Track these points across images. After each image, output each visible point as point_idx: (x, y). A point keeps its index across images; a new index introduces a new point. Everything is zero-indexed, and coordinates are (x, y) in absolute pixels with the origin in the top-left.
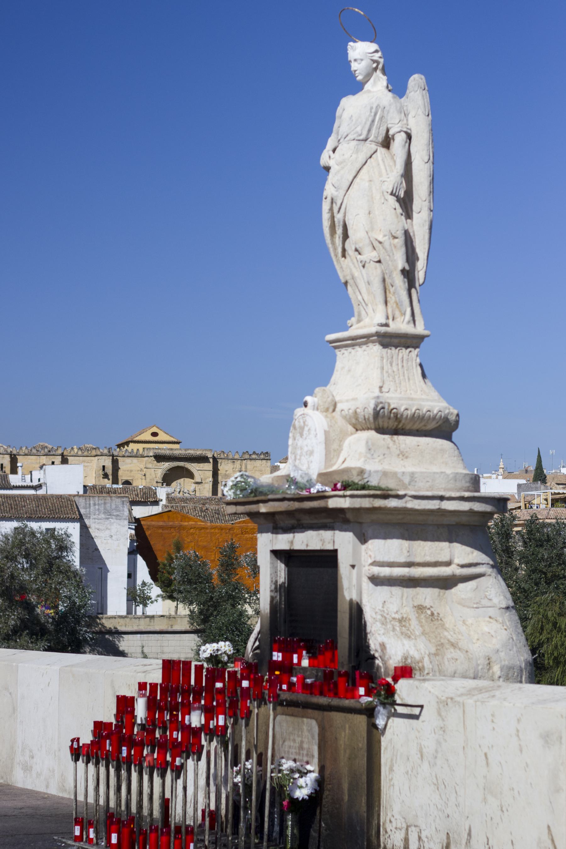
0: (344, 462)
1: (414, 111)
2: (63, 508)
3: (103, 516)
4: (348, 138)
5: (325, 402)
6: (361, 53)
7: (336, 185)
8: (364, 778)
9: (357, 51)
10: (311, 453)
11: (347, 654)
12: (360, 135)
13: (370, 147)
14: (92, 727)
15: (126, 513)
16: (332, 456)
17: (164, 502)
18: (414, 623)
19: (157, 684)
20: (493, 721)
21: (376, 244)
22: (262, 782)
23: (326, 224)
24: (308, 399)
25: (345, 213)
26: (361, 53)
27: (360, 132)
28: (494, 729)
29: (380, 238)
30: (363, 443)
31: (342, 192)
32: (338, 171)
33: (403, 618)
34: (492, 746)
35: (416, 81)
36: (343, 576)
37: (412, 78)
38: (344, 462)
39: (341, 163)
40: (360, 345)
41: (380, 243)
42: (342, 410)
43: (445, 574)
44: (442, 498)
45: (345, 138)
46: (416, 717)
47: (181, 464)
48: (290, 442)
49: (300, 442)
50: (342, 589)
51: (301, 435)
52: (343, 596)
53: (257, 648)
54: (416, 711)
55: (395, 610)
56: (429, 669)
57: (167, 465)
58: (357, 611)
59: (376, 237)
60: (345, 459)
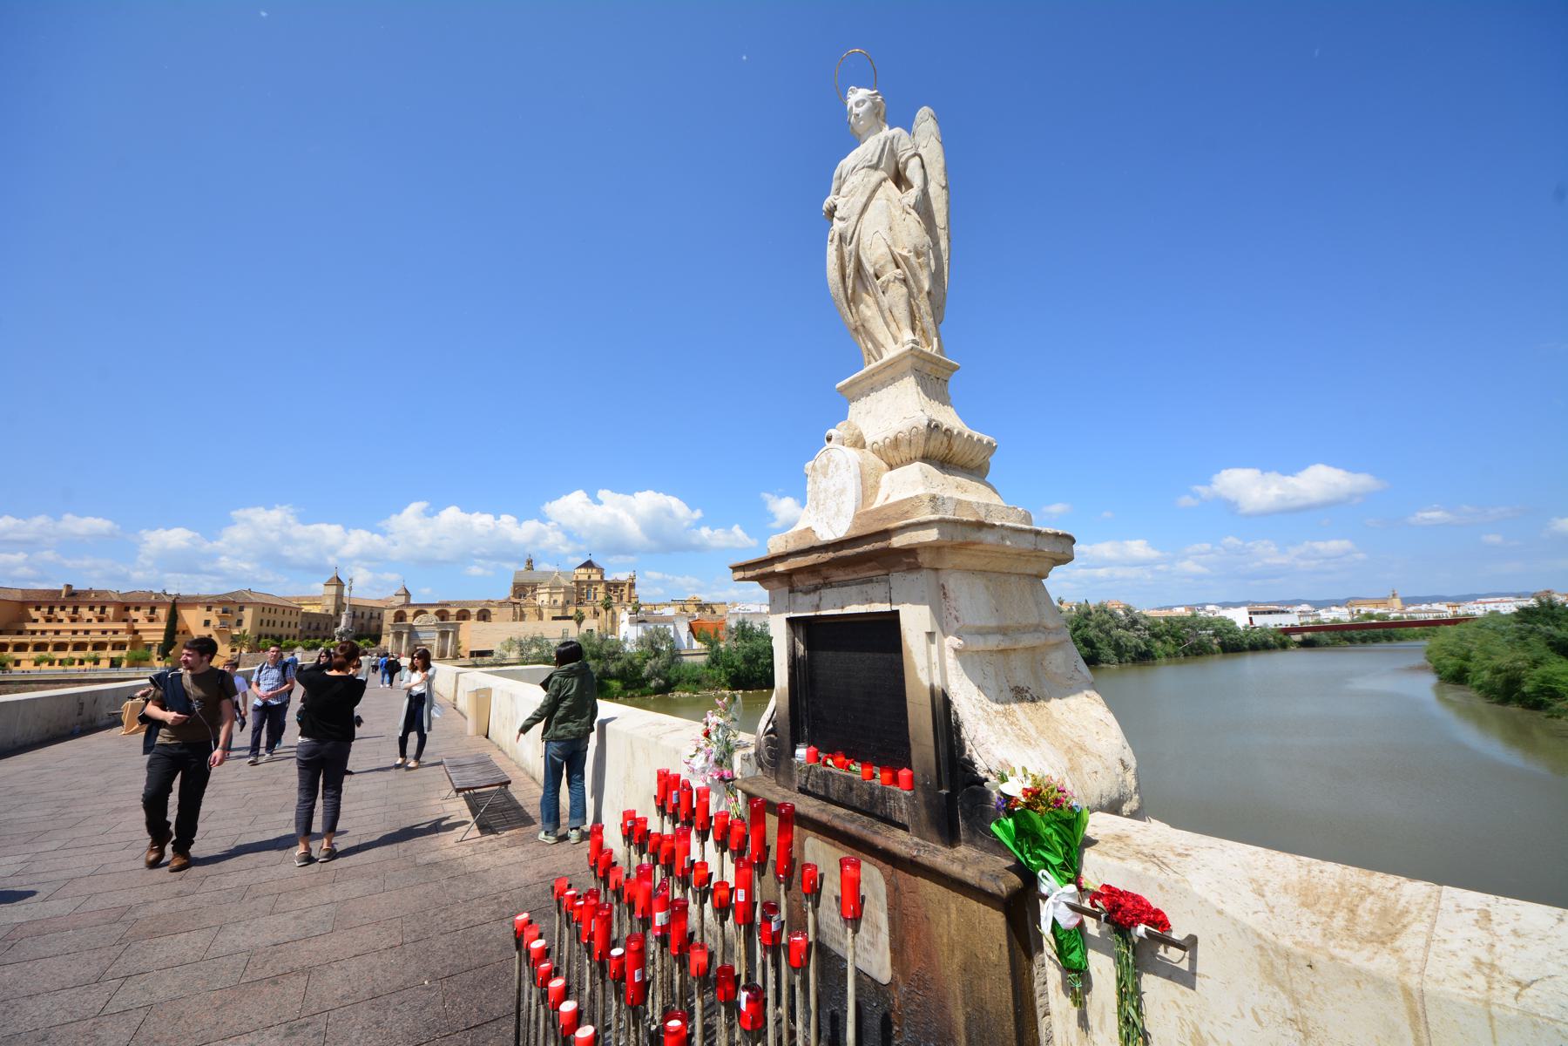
1: (924, 142)
2: (669, 620)
6: (858, 98)
8: (1010, 1026)
10: (842, 492)
11: (934, 773)
13: (881, 174)
14: (654, 788)
22: (827, 1032)
23: (832, 273)
24: (832, 431)
25: (858, 245)
26: (858, 98)
29: (905, 253)
35: (924, 112)
36: (914, 649)
40: (884, 385)
43: (36, 591)
48: (809, 488)
49: (823, 483)
50: (914, 668)
51: (825, 475)
52: (918, 681)
53: (771, 732)
58: (942, 706)
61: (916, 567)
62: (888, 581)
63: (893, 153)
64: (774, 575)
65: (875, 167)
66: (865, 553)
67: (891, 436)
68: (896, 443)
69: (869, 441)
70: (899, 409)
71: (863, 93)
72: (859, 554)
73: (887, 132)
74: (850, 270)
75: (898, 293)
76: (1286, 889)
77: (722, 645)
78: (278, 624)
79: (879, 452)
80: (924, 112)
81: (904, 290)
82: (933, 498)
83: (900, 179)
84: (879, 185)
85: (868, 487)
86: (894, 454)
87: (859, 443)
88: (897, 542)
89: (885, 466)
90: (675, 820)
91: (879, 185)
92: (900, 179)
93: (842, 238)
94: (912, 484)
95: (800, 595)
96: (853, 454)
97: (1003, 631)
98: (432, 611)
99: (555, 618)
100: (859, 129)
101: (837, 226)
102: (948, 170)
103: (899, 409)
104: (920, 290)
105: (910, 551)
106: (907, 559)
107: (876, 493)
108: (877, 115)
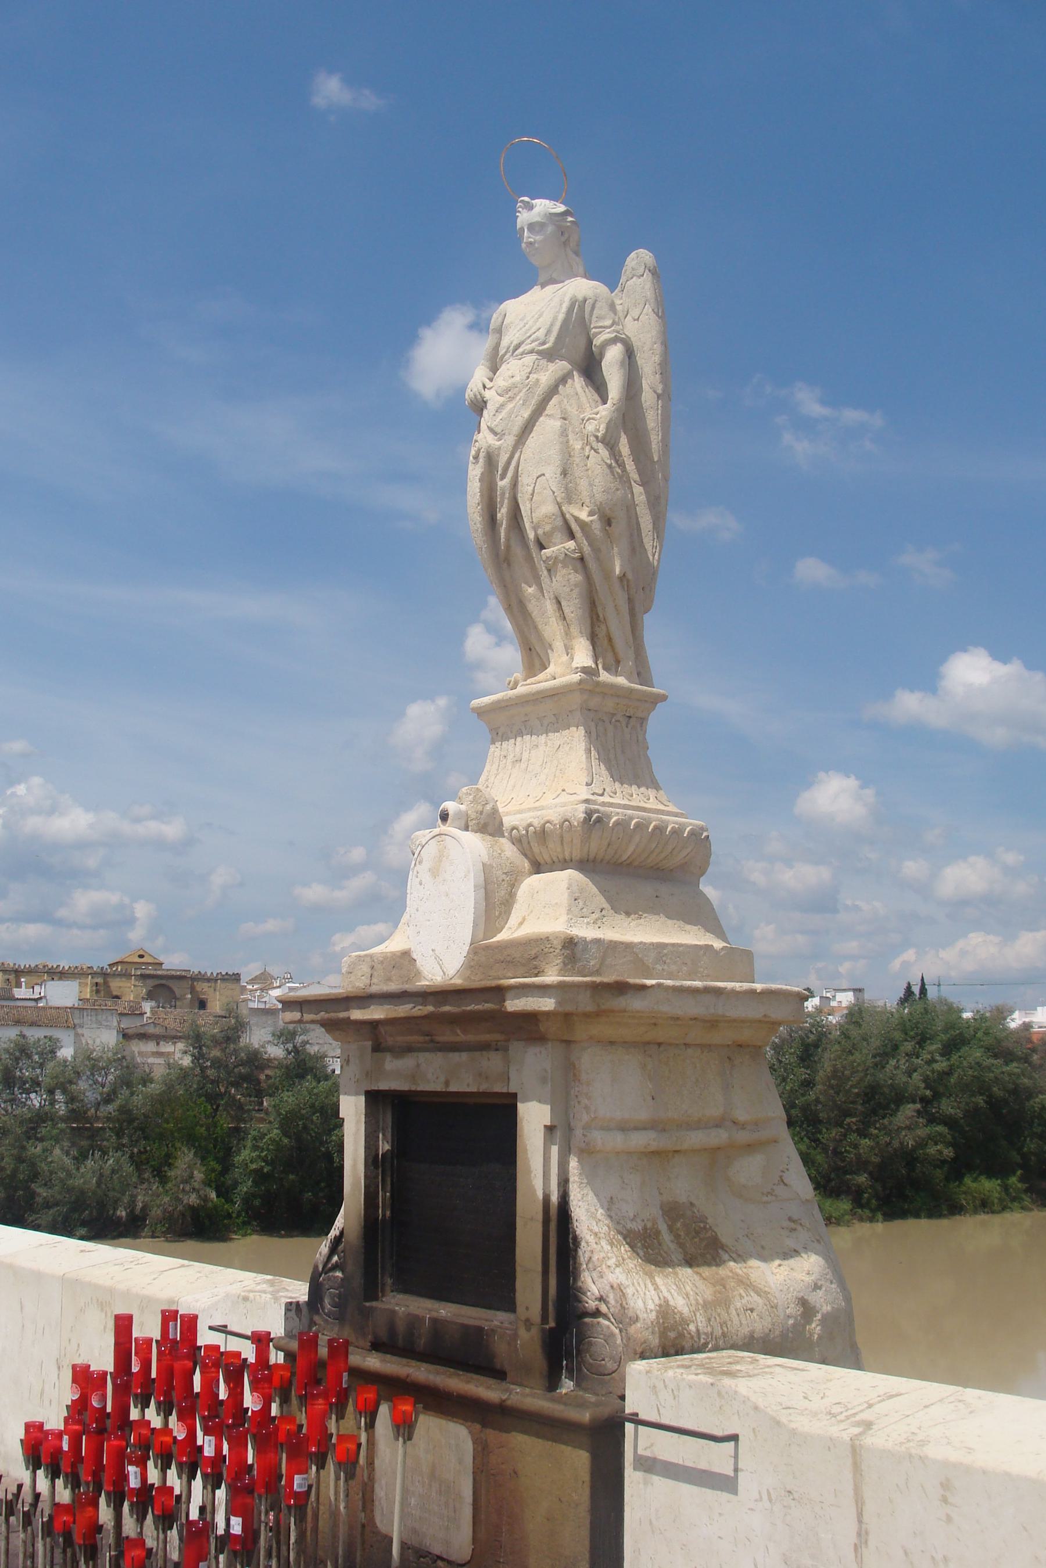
0: (521, 923)
1: (631, 311)
3: (94, 1026)
4: (520, 350)
5: (481, 813)
7: (498, 430)
9: (536, 210)
12: (544, 343)
15: (115, 1024)
16: (497, 913)
17: (148, 1015)
18: (666, 1237)
19: (105, 1373)
20: (945, 1500)
27: (542, 338)
28: (949, 1519)
29: (583, 515)
30: (565, 885)
31: (510, 440)
32: (502, 406)
33: (645, 1228)
34: (946, 1559)
37: (633, 255)
38: (521, 923)
39: (508, 390)
42: (512, 829)
45: (514, 351)
46: (727, 1484)
47: (163, 982)
52: (532, 1190)
54: (715, 1458)
55: (631, 1215)
56: (705, 1334)
57: (151, 983)
58: (560, 1223)
59: (576, 513)
60: (524, 919)
61: (540, 1039)
62: (506, 1049)
63: (583, 324)
64: (348, 1021)
65: (550, 355)
66: (471, 1012)
67: (536, 823)
68: (542, 834)
69: (508, 821)
70: (550, 780)
71: (543, 207)
72: (464, 1013)
73: (581, 287)
74: (503, 513)
75: (566, 582)
76: (690, 1387)
77: (243, 1055)
79: (517, 841)
80: (639, 259)
81: (579, 578)
82: (570, 944)
83: (590, 368)
84: (553, 391)
85: (495, 899)
86: (540, 850)
87: (488, 824)
88: (514, 1005)
89: (527, 864)
90: (74, 1483)
91: (553, 391)
92: (590, 368)
93: (491, 460)
94: (550, 907)
95: (388, 1057)
96: (473, 846)
97: (654, 1125)
100: (536, 261)
101: (484, 439)
102: (665, 368)
103: (550, 780)
104: (607, 574)
105: (531, 1018)
106: (528, 1027)
107: (508, 913)
108: (565, 244)
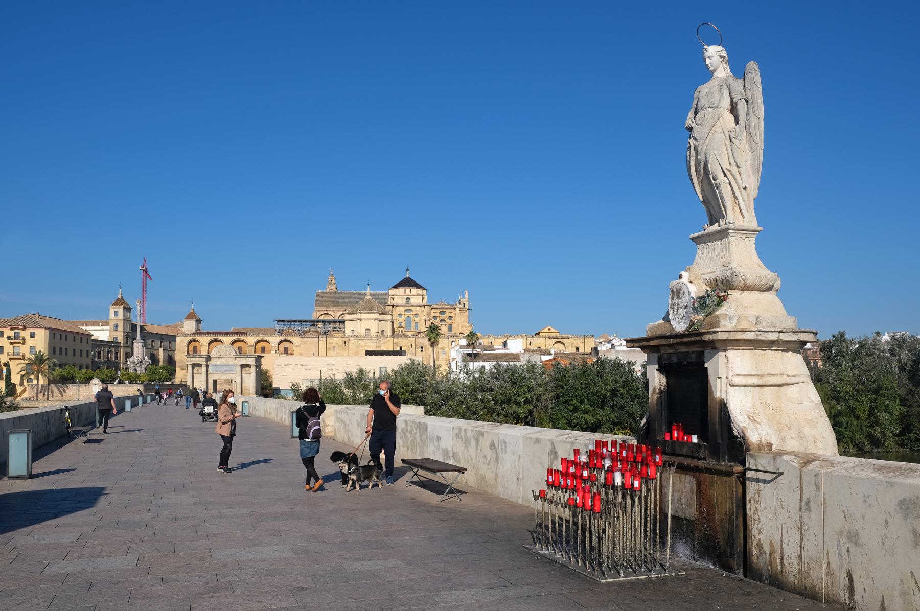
21: (726, 172)
41: (729, 171)
44: (780, 332)
58: (723, 406)
78: (70, 352)
98: (228, 340)
99: (369, 353)
